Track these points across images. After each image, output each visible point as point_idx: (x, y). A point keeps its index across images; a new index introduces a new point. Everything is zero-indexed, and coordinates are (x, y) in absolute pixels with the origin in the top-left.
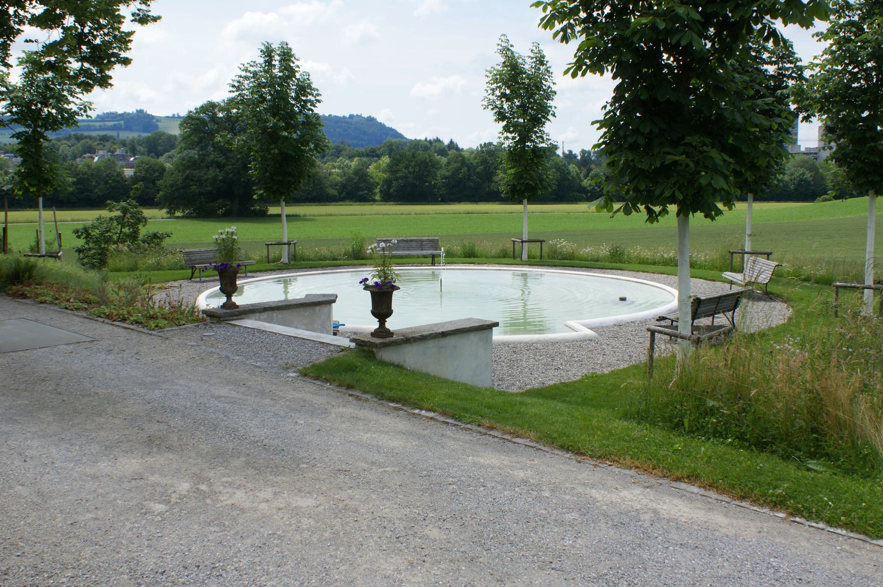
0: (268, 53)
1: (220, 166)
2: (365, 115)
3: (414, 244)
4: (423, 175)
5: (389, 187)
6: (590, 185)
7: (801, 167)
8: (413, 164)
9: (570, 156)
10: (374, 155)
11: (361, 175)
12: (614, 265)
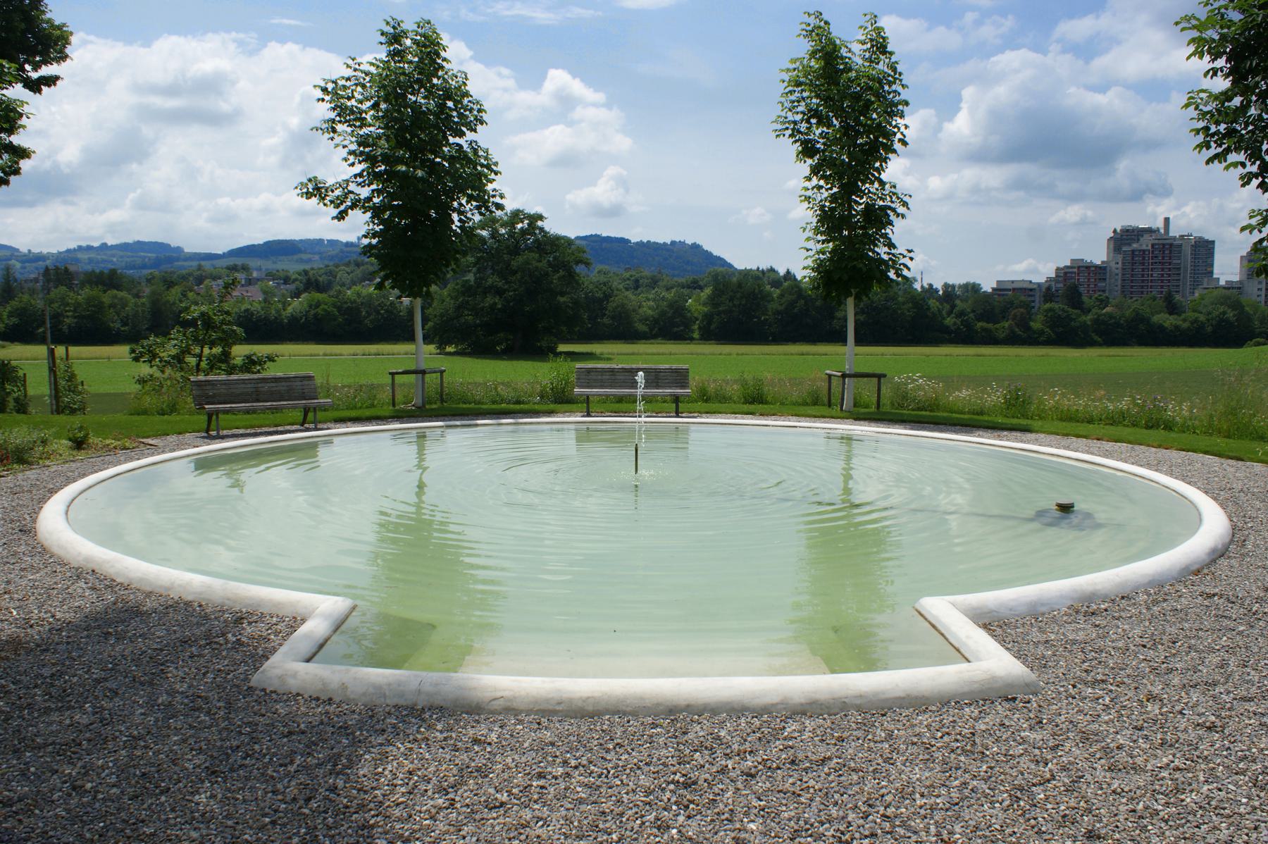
0: (395, 38)
1: (499, 292)
2: (689, 242)
5: (709, 323)
6: (955, 324)
7: (1222, 304)
8: (738, 295)
9: (931, 290)
10: (695, 286)
12: (1015, 421)
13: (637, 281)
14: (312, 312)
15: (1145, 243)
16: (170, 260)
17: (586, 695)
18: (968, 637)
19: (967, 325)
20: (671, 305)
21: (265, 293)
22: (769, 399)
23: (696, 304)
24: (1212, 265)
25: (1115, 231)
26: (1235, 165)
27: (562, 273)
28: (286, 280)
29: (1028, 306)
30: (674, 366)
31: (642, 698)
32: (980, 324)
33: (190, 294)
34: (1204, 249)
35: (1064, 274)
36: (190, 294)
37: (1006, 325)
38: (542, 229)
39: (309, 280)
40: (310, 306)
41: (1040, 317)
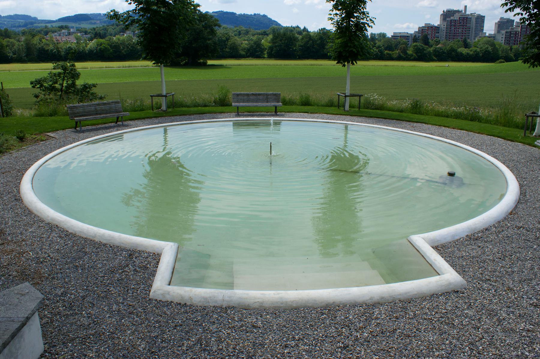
2: (262, 14)
3: (261, 97)
4: (290, 44)
5: (272, 51)
7: (487, 44)
10: (265, 34)
11: (258, 44)
13: (240, 32)
14: (99, 48)
15: (456, 17)
16: (32, 23)
17: (293, 300)
18: (435, 260)
19: (381, 52)
20: (255, 43)
21: (77, 39)
22: (312, 103)
23: (266, 42)
24: (483, 27)
25: (444, 11)
26: (518, 14)
27: (208, 30)
28: (86, 33)
29: (406, 44)
30: (274, 93)
31: (315, 300)
32: (386, 52)
33: (43, 40)
34: (480, 19)
35: (422, 30)
36: (43, 40)
37: (397, 52)
38: (199, 11)
39: (96, 33)
40: (98, 45)
41: (411, 49)
